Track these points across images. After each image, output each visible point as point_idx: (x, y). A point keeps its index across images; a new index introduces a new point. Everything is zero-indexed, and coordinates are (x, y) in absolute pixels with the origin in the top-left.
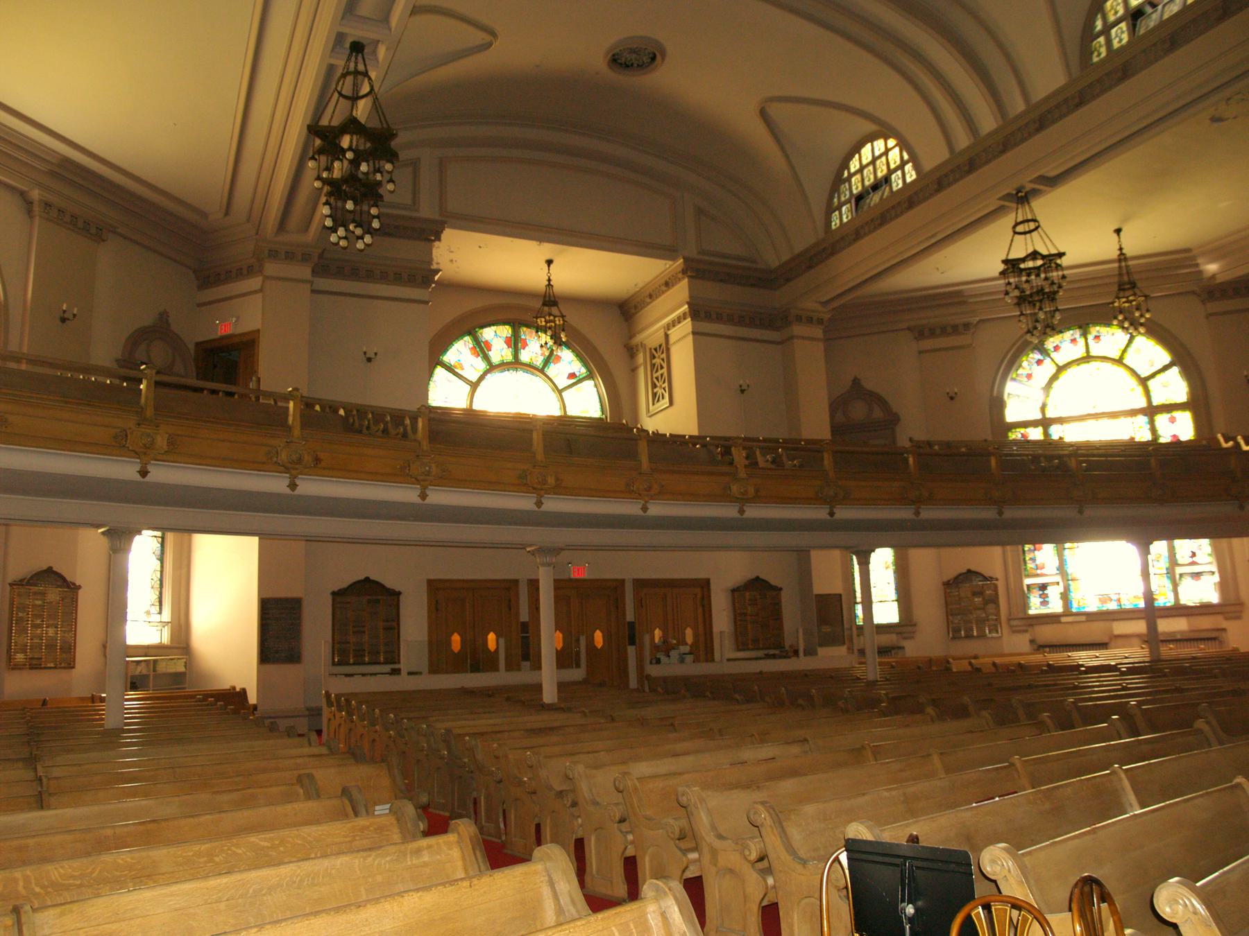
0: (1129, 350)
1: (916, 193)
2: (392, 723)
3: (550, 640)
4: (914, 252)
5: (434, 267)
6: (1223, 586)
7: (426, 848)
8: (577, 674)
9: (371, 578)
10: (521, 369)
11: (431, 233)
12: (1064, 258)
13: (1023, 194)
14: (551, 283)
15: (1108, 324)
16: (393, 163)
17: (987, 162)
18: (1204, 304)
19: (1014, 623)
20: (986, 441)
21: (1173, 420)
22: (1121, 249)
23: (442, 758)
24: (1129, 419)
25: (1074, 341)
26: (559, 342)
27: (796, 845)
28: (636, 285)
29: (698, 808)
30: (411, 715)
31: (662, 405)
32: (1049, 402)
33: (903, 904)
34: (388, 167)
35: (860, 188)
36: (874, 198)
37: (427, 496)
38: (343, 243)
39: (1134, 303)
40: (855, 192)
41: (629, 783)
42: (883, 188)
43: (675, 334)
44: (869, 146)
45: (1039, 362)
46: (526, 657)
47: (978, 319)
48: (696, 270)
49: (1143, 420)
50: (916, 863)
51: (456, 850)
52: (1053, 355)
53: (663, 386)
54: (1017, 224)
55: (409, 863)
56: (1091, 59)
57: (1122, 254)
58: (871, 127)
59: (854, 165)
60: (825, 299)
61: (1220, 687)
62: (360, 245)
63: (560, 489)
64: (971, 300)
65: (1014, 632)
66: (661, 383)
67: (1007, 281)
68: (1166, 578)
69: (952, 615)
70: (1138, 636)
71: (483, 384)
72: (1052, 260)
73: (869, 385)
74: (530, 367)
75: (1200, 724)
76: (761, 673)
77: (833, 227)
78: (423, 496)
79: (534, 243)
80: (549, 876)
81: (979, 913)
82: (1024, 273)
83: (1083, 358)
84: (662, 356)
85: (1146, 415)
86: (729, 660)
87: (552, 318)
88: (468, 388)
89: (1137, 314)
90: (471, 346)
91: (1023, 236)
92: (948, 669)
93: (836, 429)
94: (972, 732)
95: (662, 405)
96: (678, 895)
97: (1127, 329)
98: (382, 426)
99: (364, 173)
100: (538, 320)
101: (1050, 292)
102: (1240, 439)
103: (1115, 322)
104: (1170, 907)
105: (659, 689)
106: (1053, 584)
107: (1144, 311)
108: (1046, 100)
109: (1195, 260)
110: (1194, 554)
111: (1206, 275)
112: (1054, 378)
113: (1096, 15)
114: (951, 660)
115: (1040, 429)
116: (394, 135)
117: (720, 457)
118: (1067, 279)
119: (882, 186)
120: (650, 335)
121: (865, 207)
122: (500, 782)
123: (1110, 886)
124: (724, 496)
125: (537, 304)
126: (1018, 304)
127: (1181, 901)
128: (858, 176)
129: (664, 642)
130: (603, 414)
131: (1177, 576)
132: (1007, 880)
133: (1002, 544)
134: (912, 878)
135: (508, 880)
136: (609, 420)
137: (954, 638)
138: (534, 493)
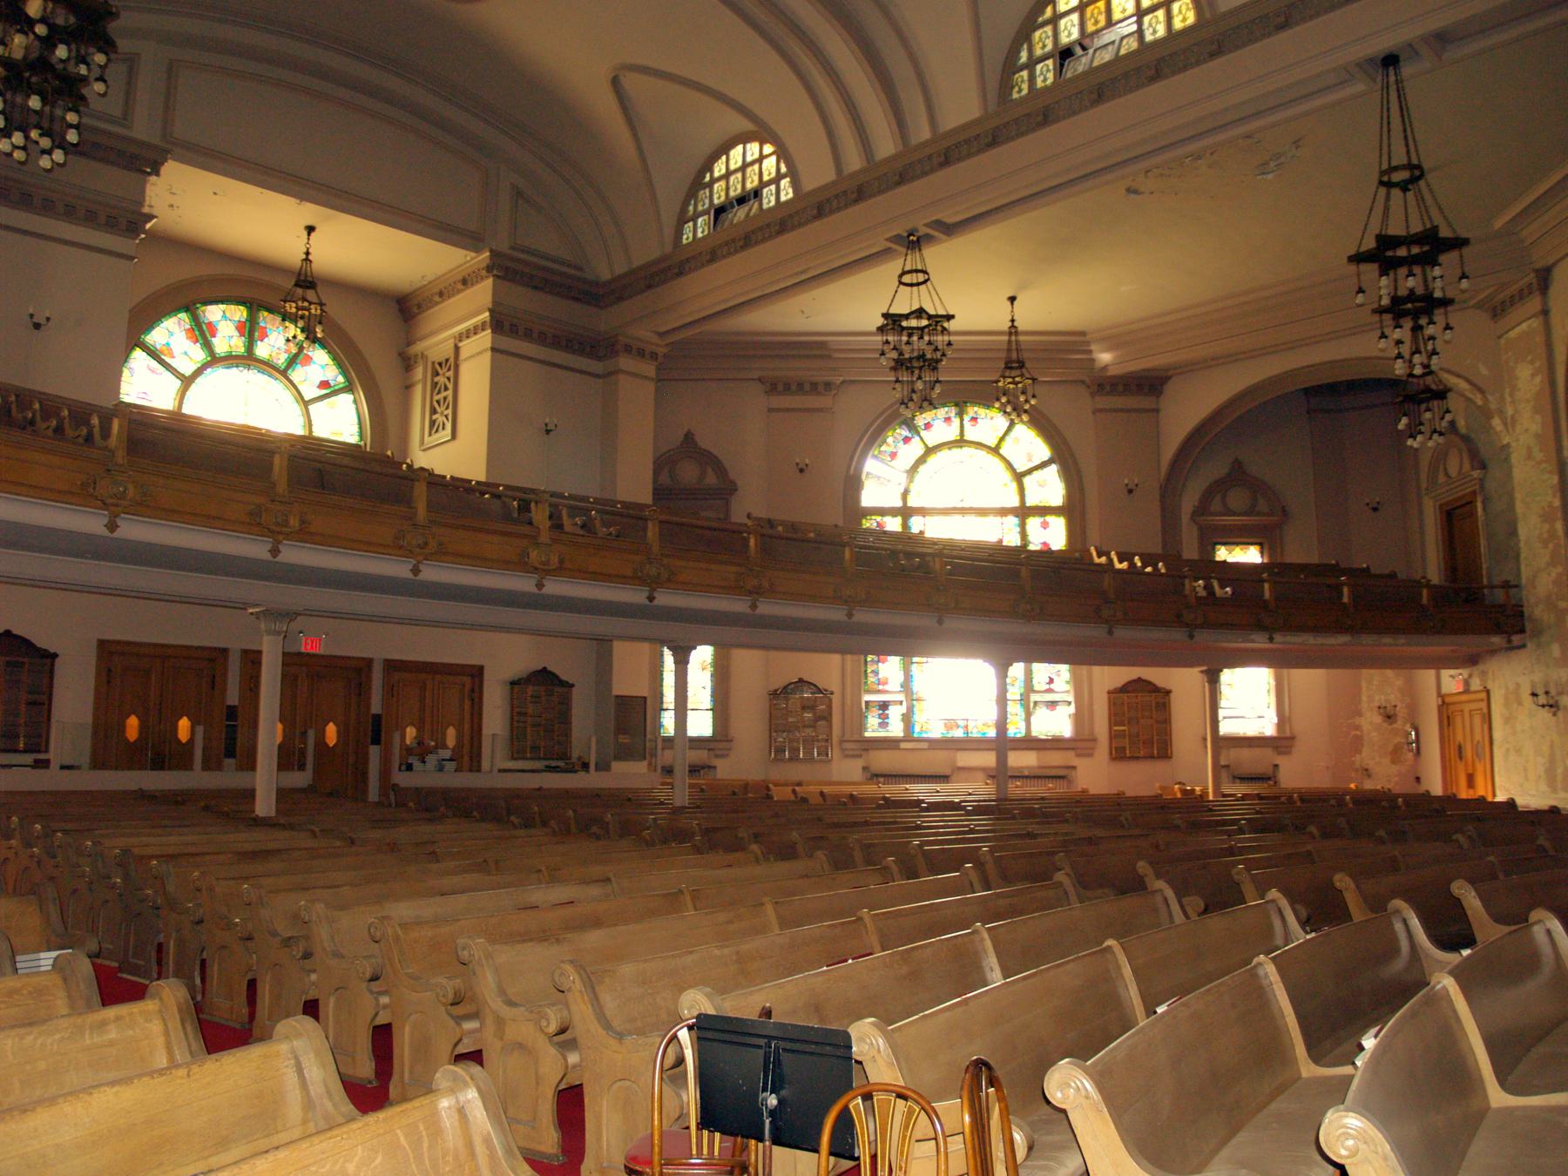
0: (1007, 438)
1: (791, 216)
2: (38, 837)
3: (269, 733)
4: (783, 285)
5: (146, 210)
6: (1078, 718)
7: (114, 1021)
8: (301, 779)
9: (15, 632)
10: (256, 367)
11: (146, 162)
12: (952, 322)
13: (915, 239)
14: (1016, 324)
15: (988, 406)
16: (106, 54)
17: (881, 192)
18: (1093, 397)
19: (848, 746)
20: (836, 526)
21: (1045, 525)
22: (1013, 321)
23: (114, 886)
24: (999, 519)
25: (948, 420)
26: (311, 336)
27: (608, 1014)
28: (423, 277)
29: (483, 966)
30: (69, 826)
31: (442, 437)
32: (913, 487)
33: (764, 1094)
34: (100, 58)
35: (723, 198)
36: (738, 214)
37: (118, 526)
38: (19, 155)
39: (1020, 385)
40: (716, 201)
41: (390, 931)
42: (752, 202)
43: (468, 347)
44: (740, 148)
45: (906, 440)
46: (230, 753)
47: (841, 379)
48: (505, 269)
49: (1012, 521)
50: (782, 1044)
51: (157, 1022)
52: (923, 433)
53: (446, 413)
54: (904, 273)
55: (88, 1042)
56: (1011, 94)
57: (1013, 326)
58: (746, 125)
59: (719, 169)
60: (663, 329)
61: (1073, 834)
62: (45, 162)
63: (305, 535)
64: (837, 355)
65: (847, 756)
66: (443, 408)
67: (885, 338)
68: (1019, 706)
69: (776, 731)
70: (984, 770)
71: (198, 380)
72: (939, 322)
73: (704, 442)
74: (267, 366)
75: (1060, 877)
76: (540, 789)
77: (685, 242)
78: (275, 552)
79: (292, 201)
80: (296, 1058)
81: (858, 1104)
82: (905, 333)
83: (956, 441)
84: (447, 374)
85: (1017, 516)
86: (500, 771)
87: (306, 304)
88: (177, 384)
89: (1022, 399)
90: (188, 327)
91: (909, 288)
92: (769, 797)
93: (658, 492)
94: (807, 876)
95: (442, 437)
96: (481, 1085)
97: (1009, 414)
98: (55, 422)
99: (61, 61)
100: (287, 305)
101: (932, 359)
102: (1113, 555)
103: (997, 405)
104: (1061, 1091)
105: (411, 804)
106: (895, 702)
107: (1030, 397)
108: (956, 131)
109: (1089, 346)
110: (1051, 681)
111: (1098, 365)
112: (921, 460)
113: (1022, 45)
114: (771, 786)
115: (899, 520)
116: (111, 14)
117: (516, 515)
118: (954, 347)
119: (749, 200)
120: (436, 344)
121: (726, 223)
122: (200, 922)
123: (999, 1072)
124: (521, 564)
125: (289, 283)
126: (894, 369)
127: (1073, 1084)
128: (723, 183)
129: (419, 744)
130: (361, 440)
131: (1032, 705)
132: (875, 1061)
133: (843, 652)
134: (778, 1062)
135: (237, 1065)
136: (368, 449)
137: (776, 760)
138: (268, 537)
